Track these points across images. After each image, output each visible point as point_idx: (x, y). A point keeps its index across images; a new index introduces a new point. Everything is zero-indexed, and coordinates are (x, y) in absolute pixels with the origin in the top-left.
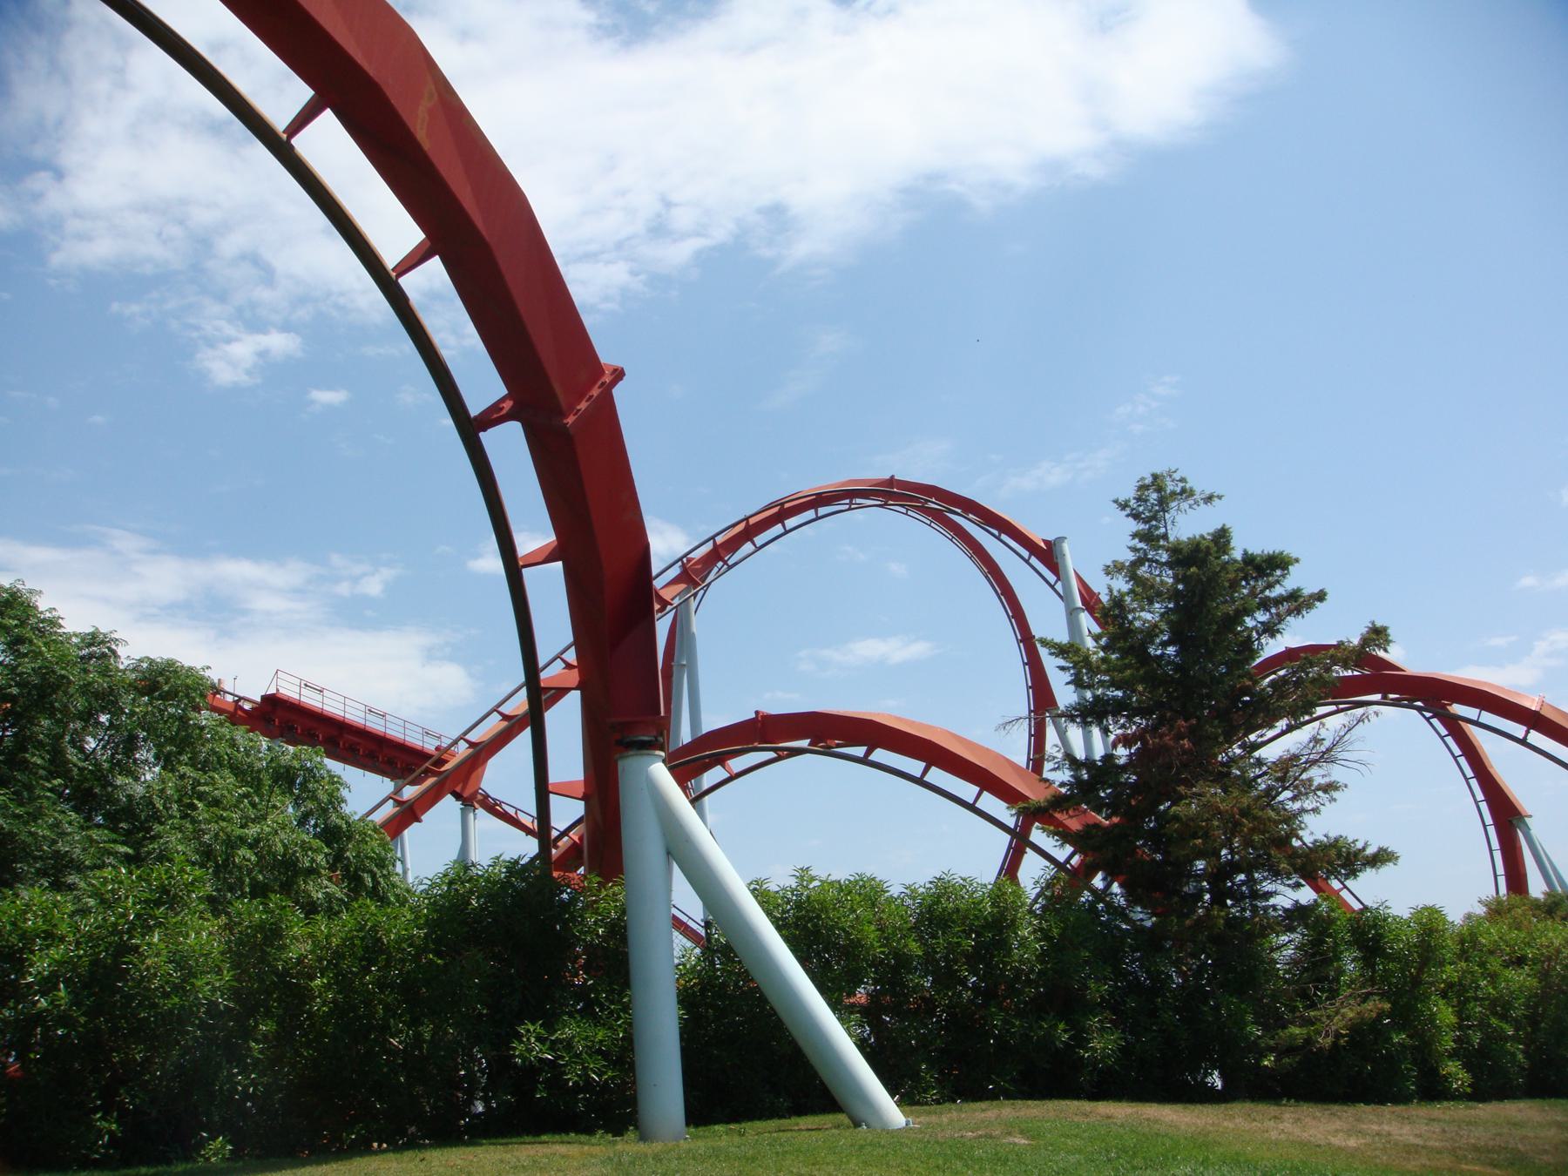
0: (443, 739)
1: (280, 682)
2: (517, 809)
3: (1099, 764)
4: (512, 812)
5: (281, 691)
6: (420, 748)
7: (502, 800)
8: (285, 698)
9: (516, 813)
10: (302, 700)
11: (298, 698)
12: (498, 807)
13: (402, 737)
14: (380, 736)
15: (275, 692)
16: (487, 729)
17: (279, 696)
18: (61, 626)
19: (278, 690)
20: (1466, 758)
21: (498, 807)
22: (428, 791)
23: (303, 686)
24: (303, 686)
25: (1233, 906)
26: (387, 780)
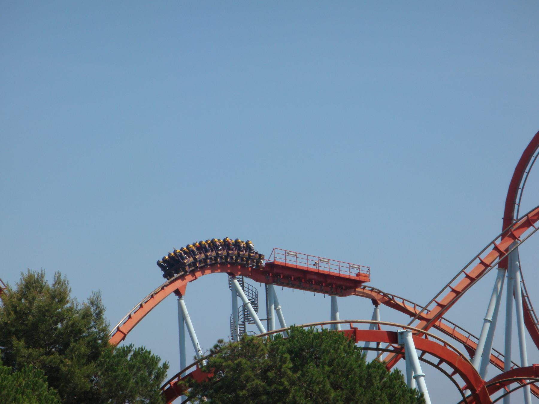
0: (361, 268)
1: (276, 255)
2: (403, 300)
3: (199, 245)
4: (399, 302)
5: (276, 260)
6: (348, 277)
7: (393, 294)
8: (279, 264)
9: (403, 302)
10: (309, 267)
11: (328, 270)
12: (392, 301)
13: (327, 270)
14: (338, 276)
15: (273, 260)
16: (495, 262)
17: (276, 263)
18: (161, 367)
19: (275, 260)
20: (515, 202)
21: (392, 301)
22: (302, 288)
23: (287, 254)
24: (287, 254)
25: (221, 250)
26: (327, 295)
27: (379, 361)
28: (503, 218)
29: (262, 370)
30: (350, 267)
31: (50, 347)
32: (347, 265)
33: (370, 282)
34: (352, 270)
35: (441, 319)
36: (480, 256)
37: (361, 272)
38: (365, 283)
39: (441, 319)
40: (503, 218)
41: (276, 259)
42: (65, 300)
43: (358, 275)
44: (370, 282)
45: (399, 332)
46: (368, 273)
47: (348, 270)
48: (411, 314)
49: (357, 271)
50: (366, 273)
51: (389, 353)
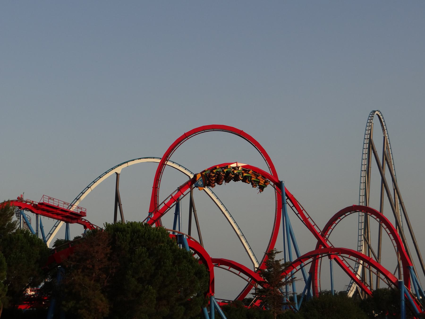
19: (44, 201)
27: (247, 181)
28: (174, 214)
29: (280, 294)
30: (49, 199)
31: (265, 281)
32: (63, 203)
33: (86, 216)
34: (65, 205)
35: (358, 251)
36: (165, 202)
37: (83, 211)
38: (84, 217)
39: (358, 251)
40: (174, 214)
41: (44, 201)
42: (7, 220)
43: (81, 212)
44: (86, 216)
45: (179, 235)
46: (85, 212)
47: (48, 200)
48: (353, 289)
49: (80, 210)
50: (84, 211)
51: (294, 272)
